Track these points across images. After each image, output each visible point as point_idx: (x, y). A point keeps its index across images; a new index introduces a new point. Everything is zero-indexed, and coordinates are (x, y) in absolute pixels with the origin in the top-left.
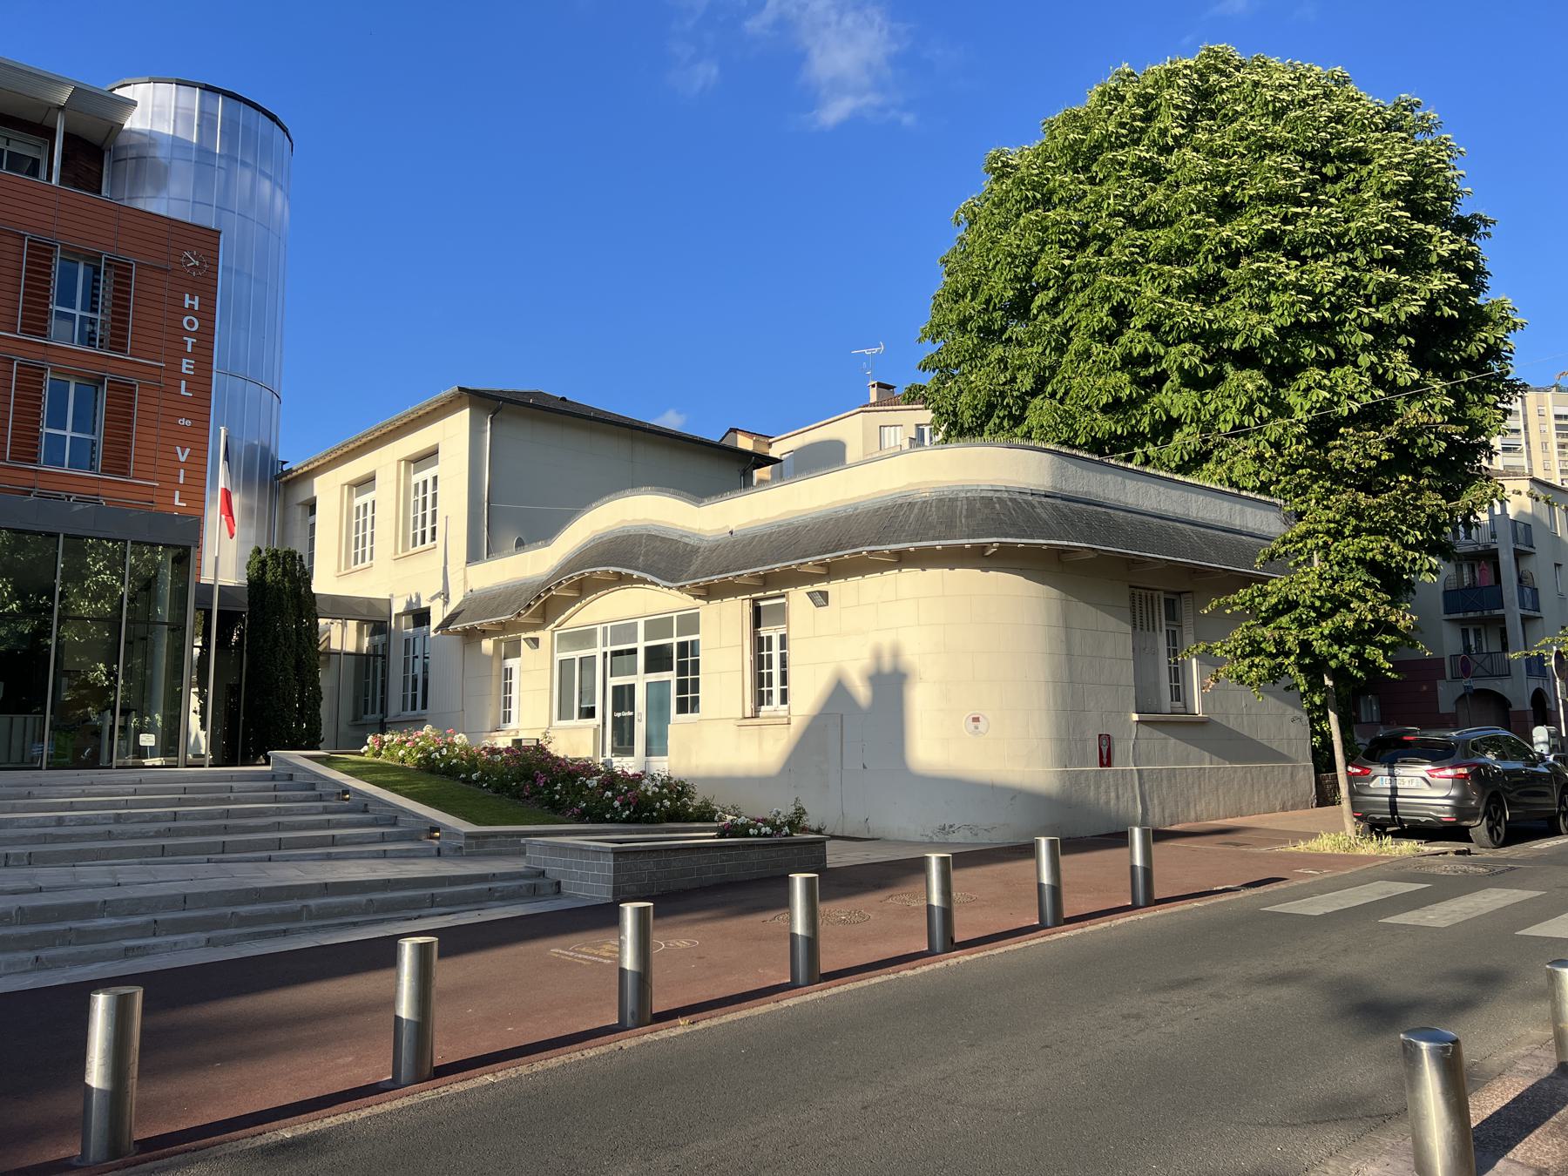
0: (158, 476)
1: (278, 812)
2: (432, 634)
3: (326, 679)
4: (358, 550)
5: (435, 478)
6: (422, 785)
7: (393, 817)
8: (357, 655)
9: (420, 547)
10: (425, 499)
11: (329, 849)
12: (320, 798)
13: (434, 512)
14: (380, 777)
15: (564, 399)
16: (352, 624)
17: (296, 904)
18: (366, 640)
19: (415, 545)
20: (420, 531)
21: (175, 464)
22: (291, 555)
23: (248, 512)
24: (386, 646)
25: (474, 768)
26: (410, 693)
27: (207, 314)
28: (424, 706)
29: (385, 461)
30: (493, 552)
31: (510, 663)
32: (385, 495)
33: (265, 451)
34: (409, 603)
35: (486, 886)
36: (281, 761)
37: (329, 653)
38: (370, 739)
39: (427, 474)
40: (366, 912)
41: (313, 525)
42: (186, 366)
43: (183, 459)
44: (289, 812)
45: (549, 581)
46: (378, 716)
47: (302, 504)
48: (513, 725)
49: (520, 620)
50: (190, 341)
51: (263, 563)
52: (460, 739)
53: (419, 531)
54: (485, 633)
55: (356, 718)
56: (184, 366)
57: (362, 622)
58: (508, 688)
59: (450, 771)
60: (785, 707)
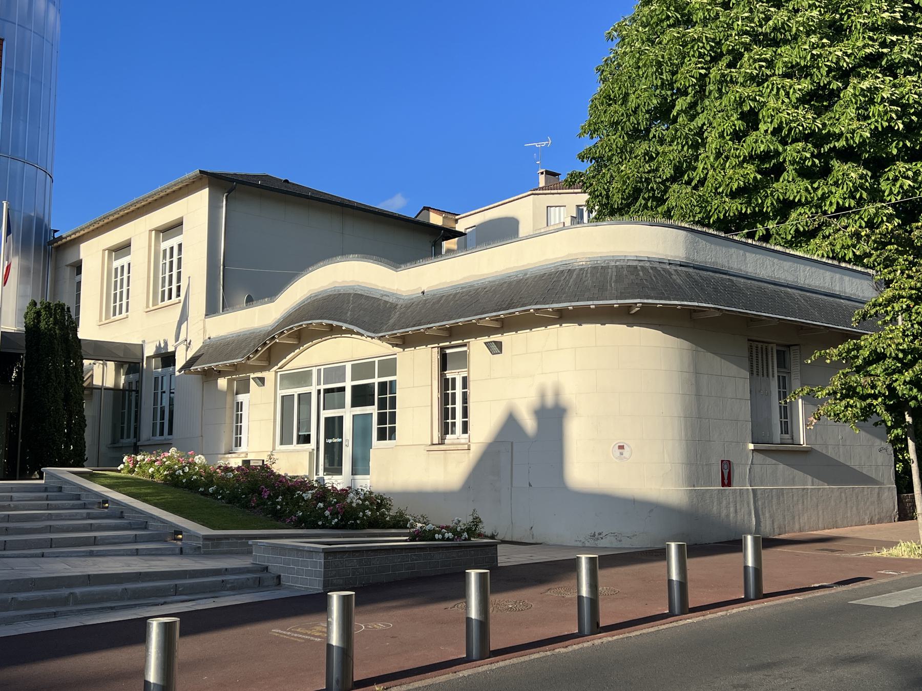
1: (50, 517)
2: (177, 374)
3: (89, 410)
4: (116, 303)
5: (180, 246)
6: (168, 497)
7: (144, 522)
8: (115, 390)
10: (171, 263)
11: (91, 547)
12: (84, 506)
13: (179, 274)
14: (133, 490)
15: (286, 181)
16: (111, 365)
17: (65, 592)
18: (123, 377)
19: (114, 314)
20: (168, 287)
22: (61, 306)
23: (24, 272)
24: (139, 382)
25: (211, 483)
26: (159, 421)
28: (170, 432)
29: (138, 231)
30: (228, 306)
31: (241, 398)
32: (139, 259)
33: (40, 223)
34: (158, 348)
35: (220, 578)
36: (52, 476)
37: (92, 388)
38: (125, 459)
39: (174, 242)
40: (121, 599)
41: (79, 283)
44: (59, 517)
45: (274, 330)
46: (132, 440)
47: (72, 265)
48: (243, 448)
49: (250, 362)
51: (38, 314)
52: (199, 459)
53: (167, 288)
54: (220, 373)
55: (114, 441)
57: (119, 365)
58: (239, 419)
59: (191, 485)
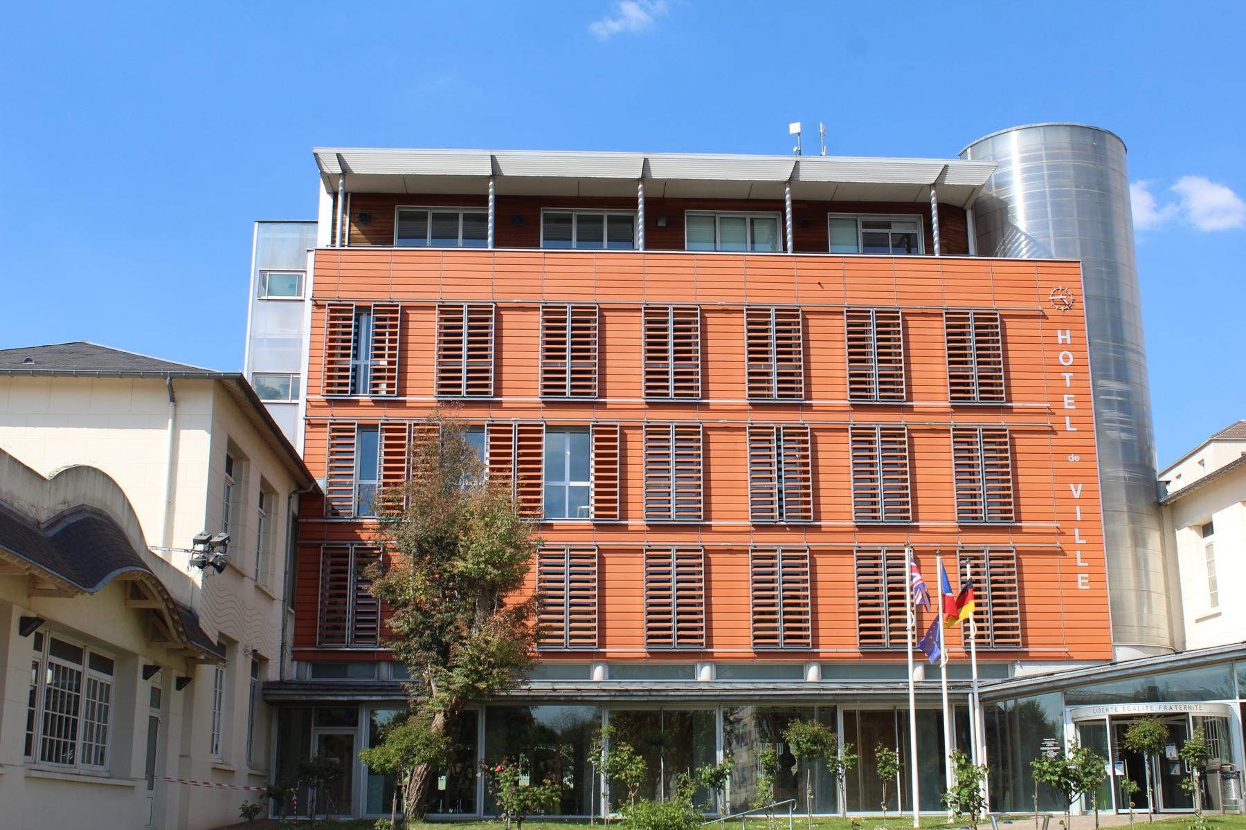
43: (1077, 495)
50: (1068, 376)
56: (1066, 402)
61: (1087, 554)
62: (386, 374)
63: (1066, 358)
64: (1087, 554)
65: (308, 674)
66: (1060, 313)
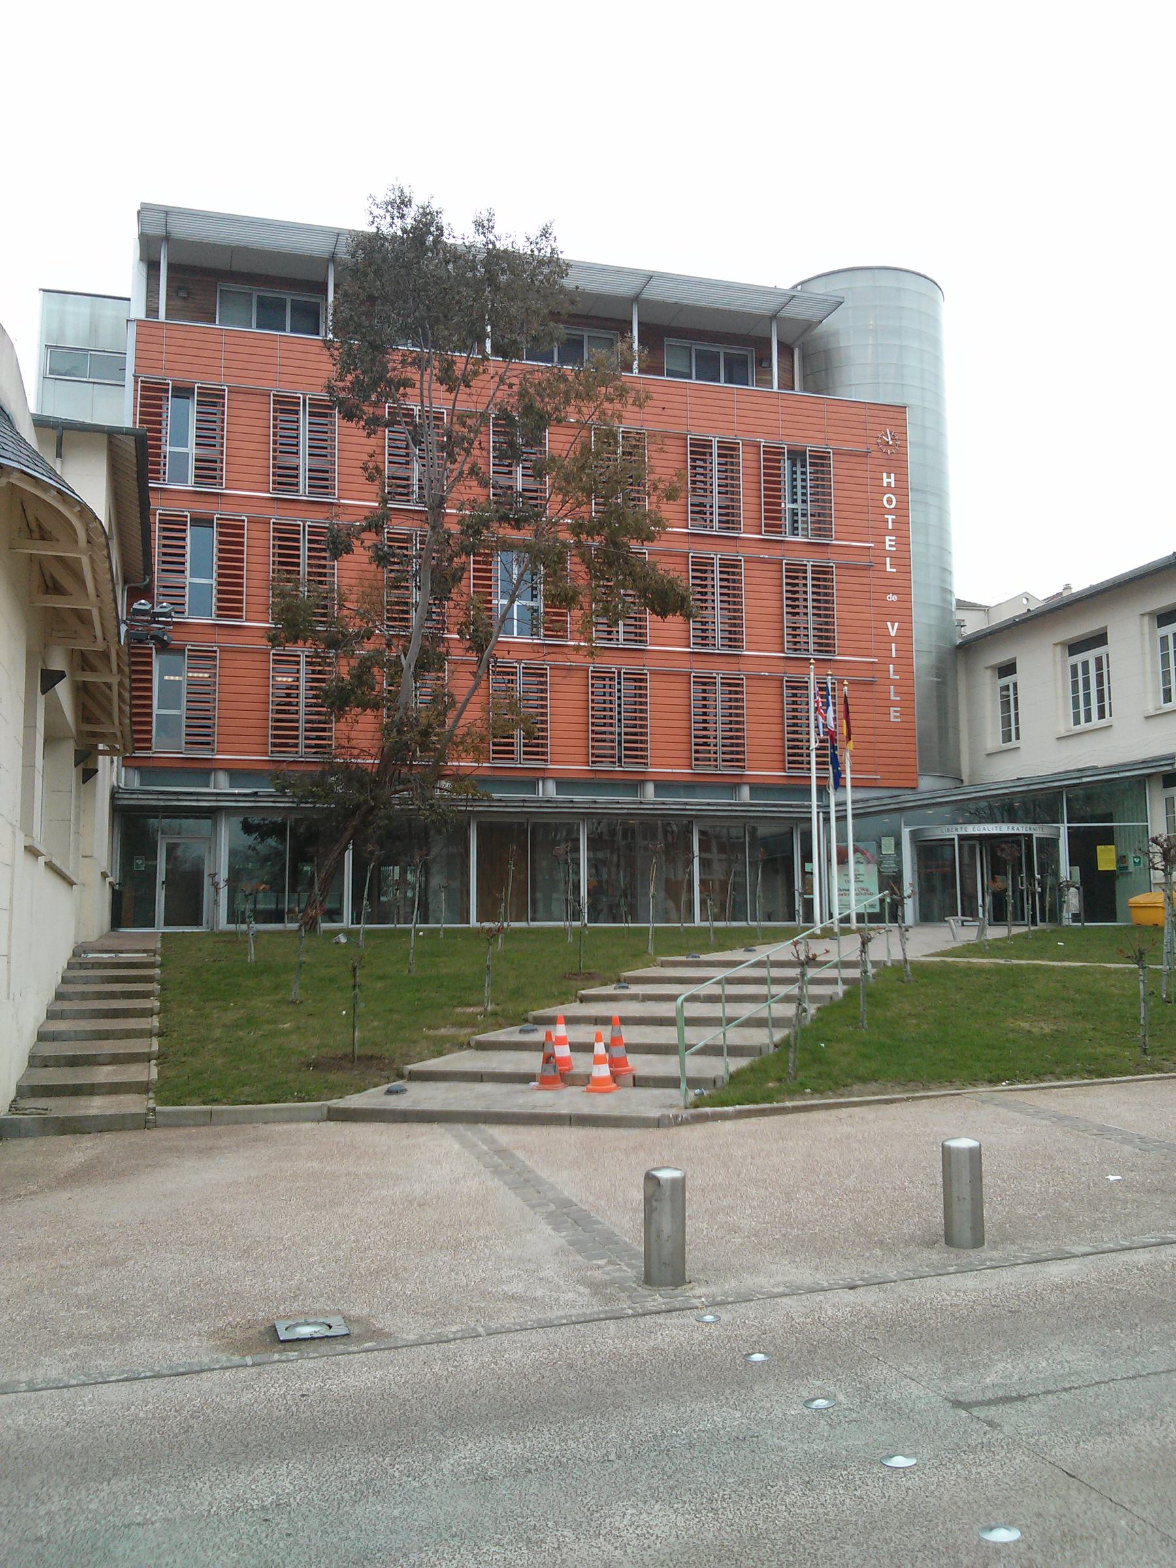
0: (875, 652)
9: (1083, 726)
21: (882, 553)
27: (901, 490)
39: (1090, 655)
42: (889, 543)
43: (893, 634)
47: (992, 667)
50: (890, 518)
56: (888, 543)
60: (1123, 853)
61: (901, 689)
62: (304, 462)
63: (890, 501)
64: (901, 689)
65: (136, 784)
66: (885, 456)
